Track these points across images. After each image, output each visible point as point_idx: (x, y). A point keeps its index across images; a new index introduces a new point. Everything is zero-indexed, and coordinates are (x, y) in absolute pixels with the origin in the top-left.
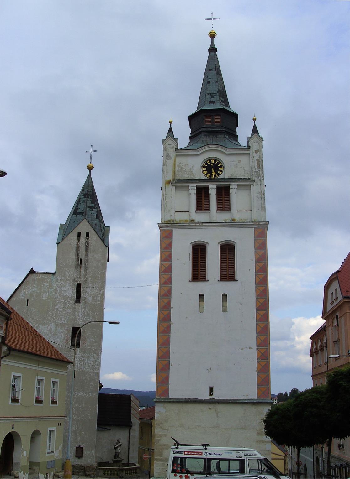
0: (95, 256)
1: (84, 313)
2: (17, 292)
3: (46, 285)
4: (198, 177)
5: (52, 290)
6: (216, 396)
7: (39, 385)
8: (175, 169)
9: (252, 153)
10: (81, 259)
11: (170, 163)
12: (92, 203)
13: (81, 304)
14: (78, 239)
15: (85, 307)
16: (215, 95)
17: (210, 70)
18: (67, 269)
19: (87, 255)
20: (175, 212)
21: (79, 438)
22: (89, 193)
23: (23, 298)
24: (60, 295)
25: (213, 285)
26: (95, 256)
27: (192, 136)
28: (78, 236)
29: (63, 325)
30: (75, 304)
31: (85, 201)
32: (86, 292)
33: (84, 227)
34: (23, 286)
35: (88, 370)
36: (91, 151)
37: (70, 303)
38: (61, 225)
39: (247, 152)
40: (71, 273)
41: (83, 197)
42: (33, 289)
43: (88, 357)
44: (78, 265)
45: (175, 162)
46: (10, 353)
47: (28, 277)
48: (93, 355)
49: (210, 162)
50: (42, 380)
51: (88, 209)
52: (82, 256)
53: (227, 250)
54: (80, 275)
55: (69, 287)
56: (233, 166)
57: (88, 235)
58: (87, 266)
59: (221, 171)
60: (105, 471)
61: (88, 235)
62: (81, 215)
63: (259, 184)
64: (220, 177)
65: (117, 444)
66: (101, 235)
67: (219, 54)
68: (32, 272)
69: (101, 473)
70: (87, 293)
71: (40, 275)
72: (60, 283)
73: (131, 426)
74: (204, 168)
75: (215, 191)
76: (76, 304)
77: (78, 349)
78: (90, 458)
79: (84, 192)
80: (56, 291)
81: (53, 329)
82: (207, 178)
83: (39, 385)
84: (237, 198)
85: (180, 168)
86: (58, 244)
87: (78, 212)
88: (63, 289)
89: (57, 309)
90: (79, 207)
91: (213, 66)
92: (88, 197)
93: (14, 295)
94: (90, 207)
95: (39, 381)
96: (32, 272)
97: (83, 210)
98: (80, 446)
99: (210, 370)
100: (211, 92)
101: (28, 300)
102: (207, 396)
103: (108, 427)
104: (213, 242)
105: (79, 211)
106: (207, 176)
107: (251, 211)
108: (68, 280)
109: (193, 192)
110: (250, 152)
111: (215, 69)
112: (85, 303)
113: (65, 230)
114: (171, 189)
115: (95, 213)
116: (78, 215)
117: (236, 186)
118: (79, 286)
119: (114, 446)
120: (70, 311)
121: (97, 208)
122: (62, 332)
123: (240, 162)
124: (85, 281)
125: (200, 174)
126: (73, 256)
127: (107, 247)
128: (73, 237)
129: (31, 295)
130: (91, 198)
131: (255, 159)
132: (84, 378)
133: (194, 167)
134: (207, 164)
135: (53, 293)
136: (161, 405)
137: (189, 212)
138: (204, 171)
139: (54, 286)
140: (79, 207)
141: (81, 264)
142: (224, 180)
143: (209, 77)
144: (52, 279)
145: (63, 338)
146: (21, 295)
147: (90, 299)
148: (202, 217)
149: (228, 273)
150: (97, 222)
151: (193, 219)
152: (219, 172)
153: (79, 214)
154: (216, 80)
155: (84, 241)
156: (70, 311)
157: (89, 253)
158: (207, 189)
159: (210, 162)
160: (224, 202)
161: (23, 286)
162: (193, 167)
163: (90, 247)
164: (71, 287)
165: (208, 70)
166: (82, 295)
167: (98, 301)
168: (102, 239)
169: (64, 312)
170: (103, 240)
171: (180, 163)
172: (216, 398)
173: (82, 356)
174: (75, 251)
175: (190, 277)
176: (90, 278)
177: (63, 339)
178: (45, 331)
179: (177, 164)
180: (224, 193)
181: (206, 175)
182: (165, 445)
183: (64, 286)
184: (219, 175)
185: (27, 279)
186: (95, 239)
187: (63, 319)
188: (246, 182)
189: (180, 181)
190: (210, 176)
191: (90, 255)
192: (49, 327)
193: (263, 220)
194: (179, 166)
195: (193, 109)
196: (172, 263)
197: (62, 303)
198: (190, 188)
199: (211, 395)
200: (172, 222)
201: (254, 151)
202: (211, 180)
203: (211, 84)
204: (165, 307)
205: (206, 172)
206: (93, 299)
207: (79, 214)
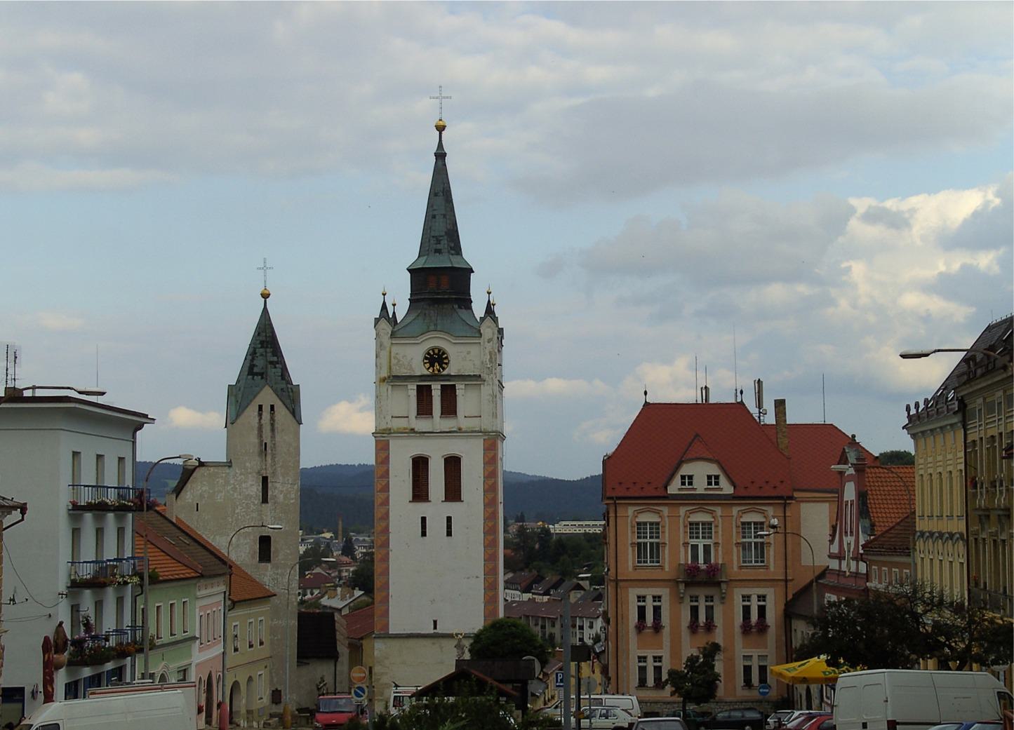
1: (274, 517)
3: (221, 481)
4: (418, 374)
6: (439, 630)
8: (390, 363)
9: (484, 342)
10: (266, 444)
11: (384, 354)
14: (260, 415)
16: (441, 238)
17: (436, 195)
19: (273, 437)
20: (392, 417)
21: (275, 680)
22: (268, 339)
23: (190, 501)
24: (240, 495)
25: (437, 507)
28: (259, 410)
30: (261, 506)
32: (276, 488)
33: (267, 396)
34: (189, 486)
36: (264, 268)
37: (254, 505)
40: (253, 463)
41: (260, 346)
42: (204, 488)
44: (261, 451)
45: (390, 353)
49: (433, 351)
51: (269, 366)
52: (267, 437)
53: (453, 464)
54: (266, 465)
56: (461, 359)
57: (272, 407)
58: (274, 452)
59: (446, 364)
60: (308, 719)
61: (272, 407)
62: (260, 377)
63: (491, 383)
64: (445, 373)
65: (320, 683)
69: (304, 721)
72: (239, 479)
73: (338, 658)
74: (426, 359)
75: (439, 393)
76: (263, 505)
77: (269, 565)
78: (291, 700)
79: (261, 338)
80: (234, 489)
84: (466, 399)
85: (396, 361)
87: (255, 371)
89: (238, 513)
90: (255, 362)
92: (267, 347)
94: (271, 363)
97: (262, 368)
98: (277, 689)
99: (433, 601)
100: (437, 234)
102: (432, 631)
103: (305, 661)
104: (437, 453)
105: (256, 370)
107: (480, 417)
108: (250, 473)
109: (413, 393)
110: (481, 341)
111: (443, 192)
112: (275, 503)
114: (385, 386)
116: (255, 377)
117: (463, 387)
118: (265, 480)
119: (317, 686)
120: (255, 515)
123: (469, 353)
124: (273, 473)
125: (421, 369)
126: (254, 439)
127: (300, 423)
129: (201, 496)
130: (271, 348)
131: (487, 351)
132: (279, 602)
133: (413, 358)
134: (429, 354)
135: (232, 492)
136: (381, 641)
137: (407, 417)
138: (426, 363)
139: (232, 482)
140: (255, 362)
142: (449, 377)
143: (435, 207)
144: (228, 473)
145: (248, 551)
146: (187, 497)
148: (423, 425)
149: (453, 492)
151: (413, 427)
152: (444, 365)
153: (257, 374)
154: (443, 212)
155: (269, 417)
156: (255, 515)
157: (276, 434)
160: (450, 409)
162: (412, 359)
163: (276, 426)
164: (254, 483)
165: (433, 194)
166: (270, 493)
167: (293, 499)
168: (292, 410)
169: (248, 517)
170: (294, 416)
171: (397, 354)
172: (440, 632)
173: (274, 573)
174: (256, 432)
175: (410, 497)
177: (249, 553)
179: (393, 354)
180: (449, 394)
182: (386, 684)
184: (444, 369)
186: (283, 413)
188: (474, 379)
189: (397, 378)
191: (278, 438)
193: (494, 429)
194: (395, 358)
196: (389, 481)
197: (244, 505)
199: (435, 628)
200: (389, 431)
201: (486, 340)
203: (437, 217)
205: (427, 365)
207: (257, 374)
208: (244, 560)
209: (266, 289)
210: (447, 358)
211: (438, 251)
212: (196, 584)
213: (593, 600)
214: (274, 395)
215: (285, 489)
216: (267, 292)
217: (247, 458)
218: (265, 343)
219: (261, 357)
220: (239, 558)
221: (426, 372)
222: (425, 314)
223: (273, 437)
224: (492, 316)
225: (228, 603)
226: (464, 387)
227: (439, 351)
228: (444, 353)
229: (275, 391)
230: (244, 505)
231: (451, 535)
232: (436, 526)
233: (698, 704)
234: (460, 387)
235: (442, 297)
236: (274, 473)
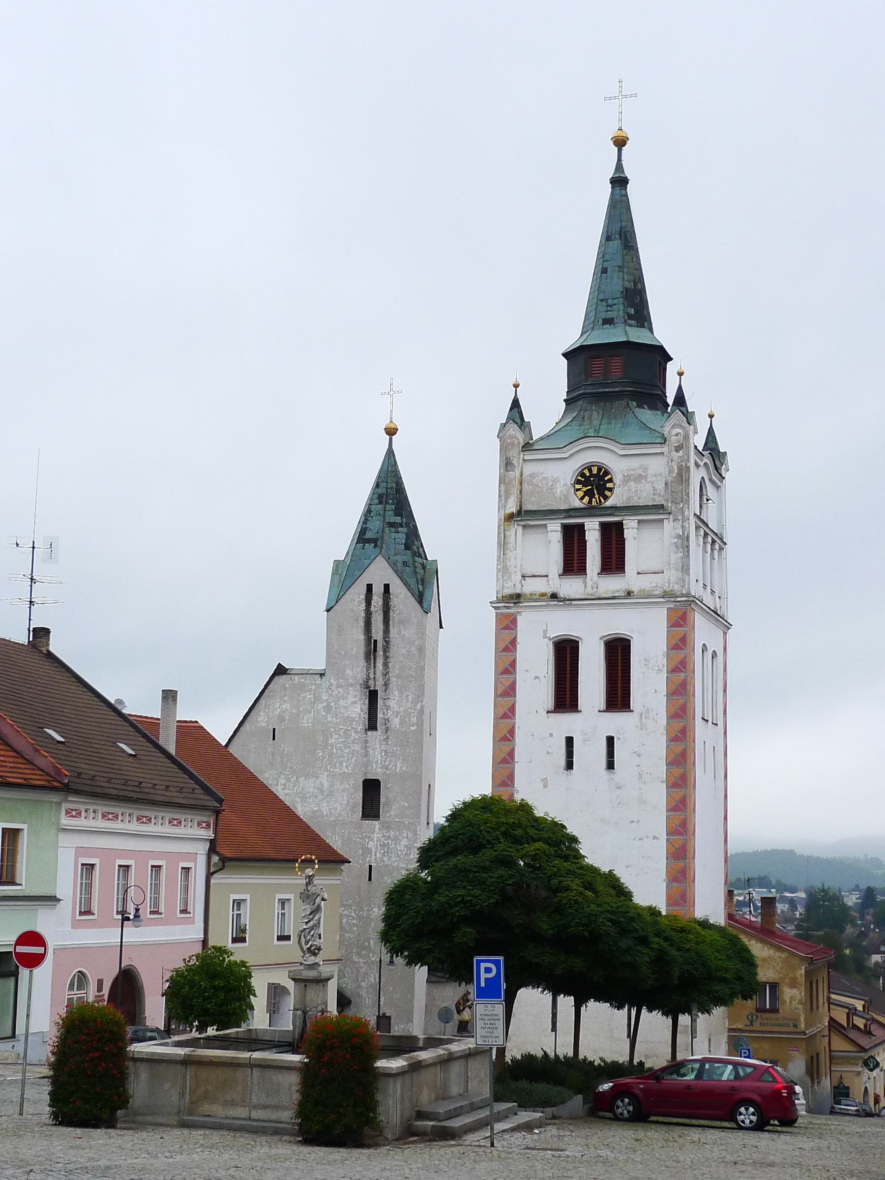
1: (385, 751)
2: (253, 713)
5: (320, 706)
7: (283, 908)
10: (375, 641)
12: (396, 515)
13: (378, 734)
15: (387, 738)
18: (348, 663)
19: (386, 631)
20: (523, 576)
23: (264, 725)
25: (591, 718)
27: (571, 399)
29: (345, 776)
31: (382, 512)
33: (379, 572)
35: (396, 864)
36: (391, 392)
37: (356, 732)
38: (337, 563)
39: (659, 451)
40: (356, 669)
43: (396, 839)
46: (224, 866)
47: (273, 683)
48: (405, 835)
49: (590, 471)
50: (288, 900)
53: (618, 652)
57: (387, 587)
61: (387, 587)
63: (680, 518)
64: (608, 503)
66: (413, 585)
67: (631, 189)
68: (281, 670)
70: (393, 707)
72: (336, 692)
76: (369, 733)
77: (377, 822)
79: (380, 491)
80: (328, 708)
81: (326, 784)
82: (582, 506)
83: (283, 908)
84: (640, 545)
86: (328, 611)
91: (617, 227)
92: (387, 503)
93: (247, 721)
94: (391, 525)
95: (283, 902)
96: (281, 670)
101: (274, 730)
104: (591, 632)
106: (584, 501)
108: (352, 685)
111: (620, 235)
113: (345, 575)
114: (516, 531)
115: (401, 537)
116: (367, 545)
117: (634, 524)
118: (373, 696)
120: (357, 747)
121: (407, 525)
122: (343, 790)
128: (358, 592)
129: (281, 719)
138: (578, 490)
139: (325, 698)
142: (615, 509)
145: (345, 802)
146: (260, 719)
147: (395, 722)
148: (572, 587)
149: (618, 697)
150: (407, 556)
152: (607, 493)
153: (369, 541)
159: (590, 471)
160: (613, 561)
161: (262, 701)
166: (380, 715)
167: (413, 726)
169: (347, 751)
174: (362, 624)
175: (550, 703)
176: (394, 679)
178: (311, 790)
181: (582, 498)
183: (344, 698)
184: (606, 498)
185: (271, 686)
187: (344, 764)
190: (590, 502)
192: (318, 782)
195: (572, 338)
197: (341, 732)
198: (549, 529)
200: (517, 598)
202: (593, 511)
204: (504, 761)
206: (402, 722)
207: (369, 541)
208: (340, 815)
209: (391, 422)
210: (611, 490)
211: (608, 321)
212: (60, 804)
214: (390, 570)
215: (402, 709)
216: (393, 426)
217: (348, 663)
218: (390, 497)
219: (378, 517)
220: (333, 812)
221: (577, 504)
222: (583, 418)
223: (386, 631)
224: (683, 409)
225: (215, 859)
226: (636, 525)
227: (599, 469)
228: (607, 473)
229: (393, 566)
230: (341, 732)
231: (613, 768)
232: (590, 754)
233: (451, 1054)
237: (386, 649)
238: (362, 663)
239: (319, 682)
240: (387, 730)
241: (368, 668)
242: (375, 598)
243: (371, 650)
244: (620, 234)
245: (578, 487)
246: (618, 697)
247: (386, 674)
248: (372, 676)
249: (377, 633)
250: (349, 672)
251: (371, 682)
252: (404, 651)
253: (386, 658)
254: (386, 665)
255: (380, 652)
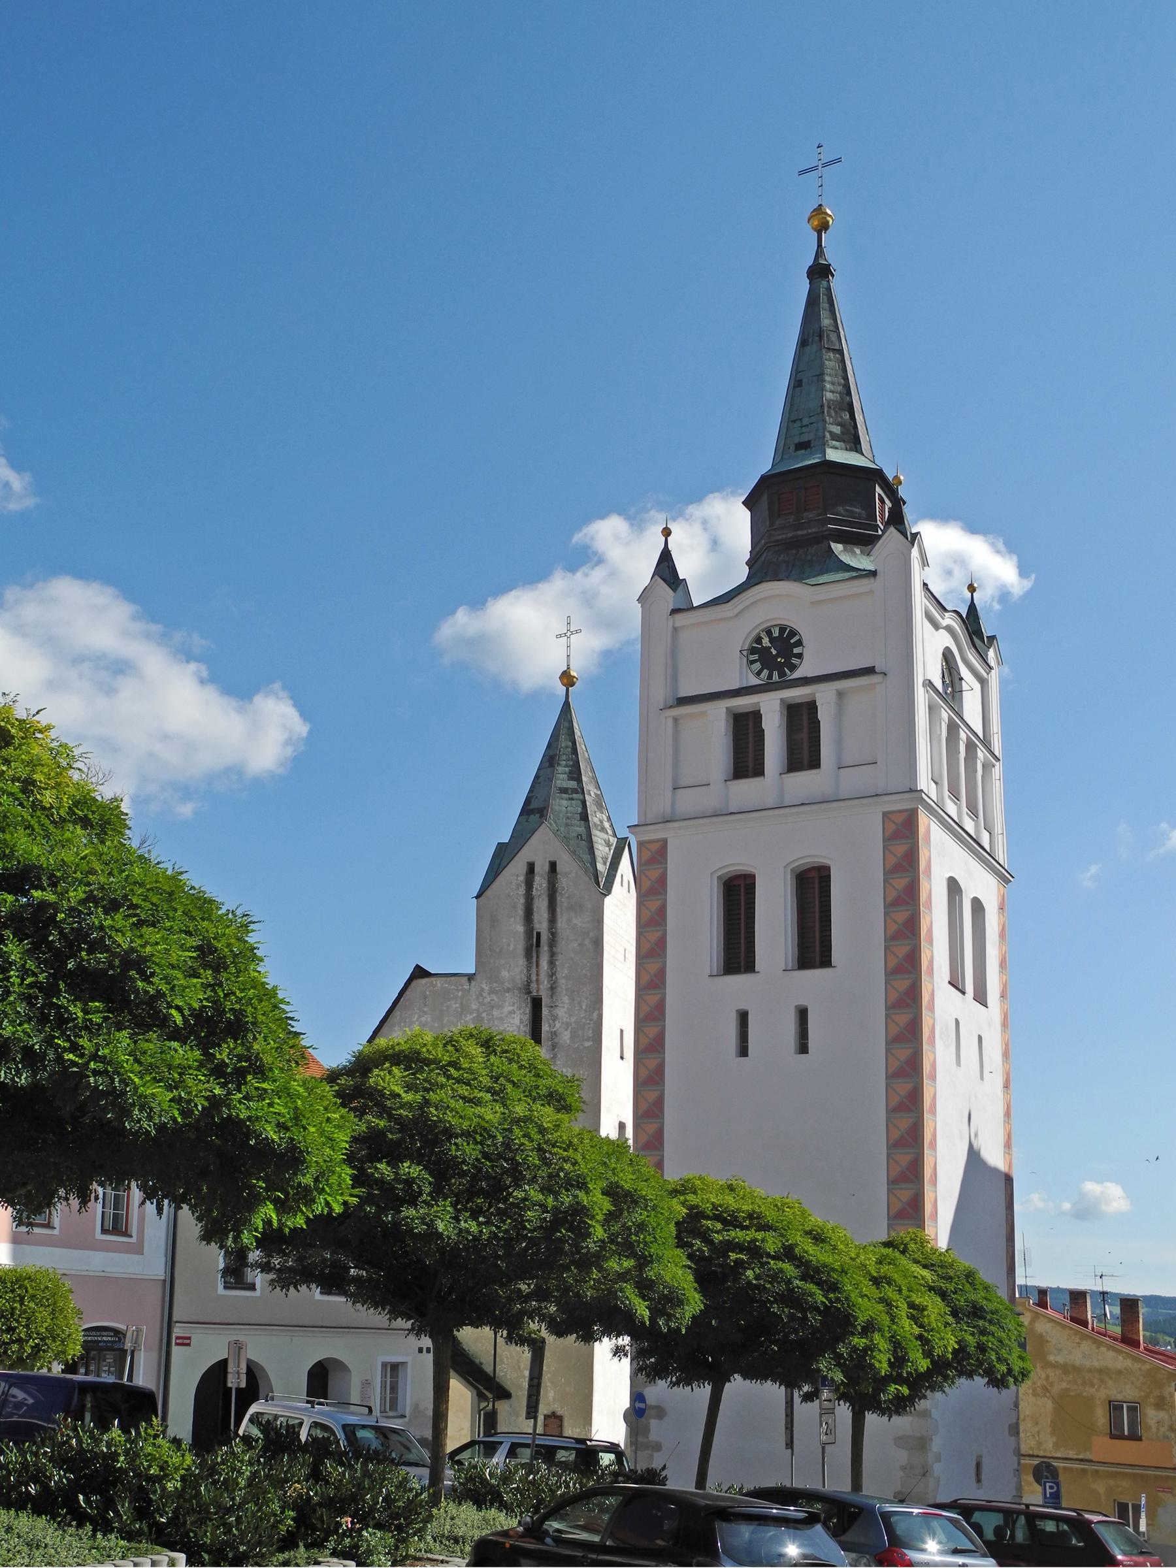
0: (575, 921)
5: (469, 1017)
6: (176, 1350)
10: (539, 934)
12: (571, 779)
19: (552, 920)
26: (575, 921)
40: (513, 969)
42: (423, 1019)
47: (409, 989)
53: (813, 886)
55: (511, 1008)
57: (553, 866)
61: (553, 866)
64: (797, 674)
67: (837, 284)
68: (419, 973)
71: (438, 982)
88: (496, 1013)
96: (419, 973)
108: (508, 990)
118: (536, 1004)
139: (474, 1007)
141: (538, 945)
147: (565, 1037)
148: (748, 788)
149: (813, 949)
152: (795, 661)
158: (756, 716)
160: (804, 752)
166: (545, 1028)
167: (588, 1040)
176: (563, 981)
180: (803, 719)
181: (759, 674)
184: (793, 668)
185: (407, 993)
190: (770, 677)
191: (561, 923)
206: (574, 1036)
213: (873, 574)
221: (755, 681)
223: (552, 920)
232: (773, 1032)
234: (824, 696)
235: (805, 532)
236: (553, 989)
237: (552, 943)
238: (522, 961)
239: (466, 987)
240: (554, 1046)
241: (529, 968)
242: (537, 879)
243: (533, 945)
244: (817, 336)
245: (752, 657)
246: (813, 949)
247: (552, 975)
248: (534, 978)
249: (541, 923)
250: (505, 974)
251: (534, 986)
252: (575, 945)
253: (552, 954)
254: (552, 963)
255: (545, 948)
